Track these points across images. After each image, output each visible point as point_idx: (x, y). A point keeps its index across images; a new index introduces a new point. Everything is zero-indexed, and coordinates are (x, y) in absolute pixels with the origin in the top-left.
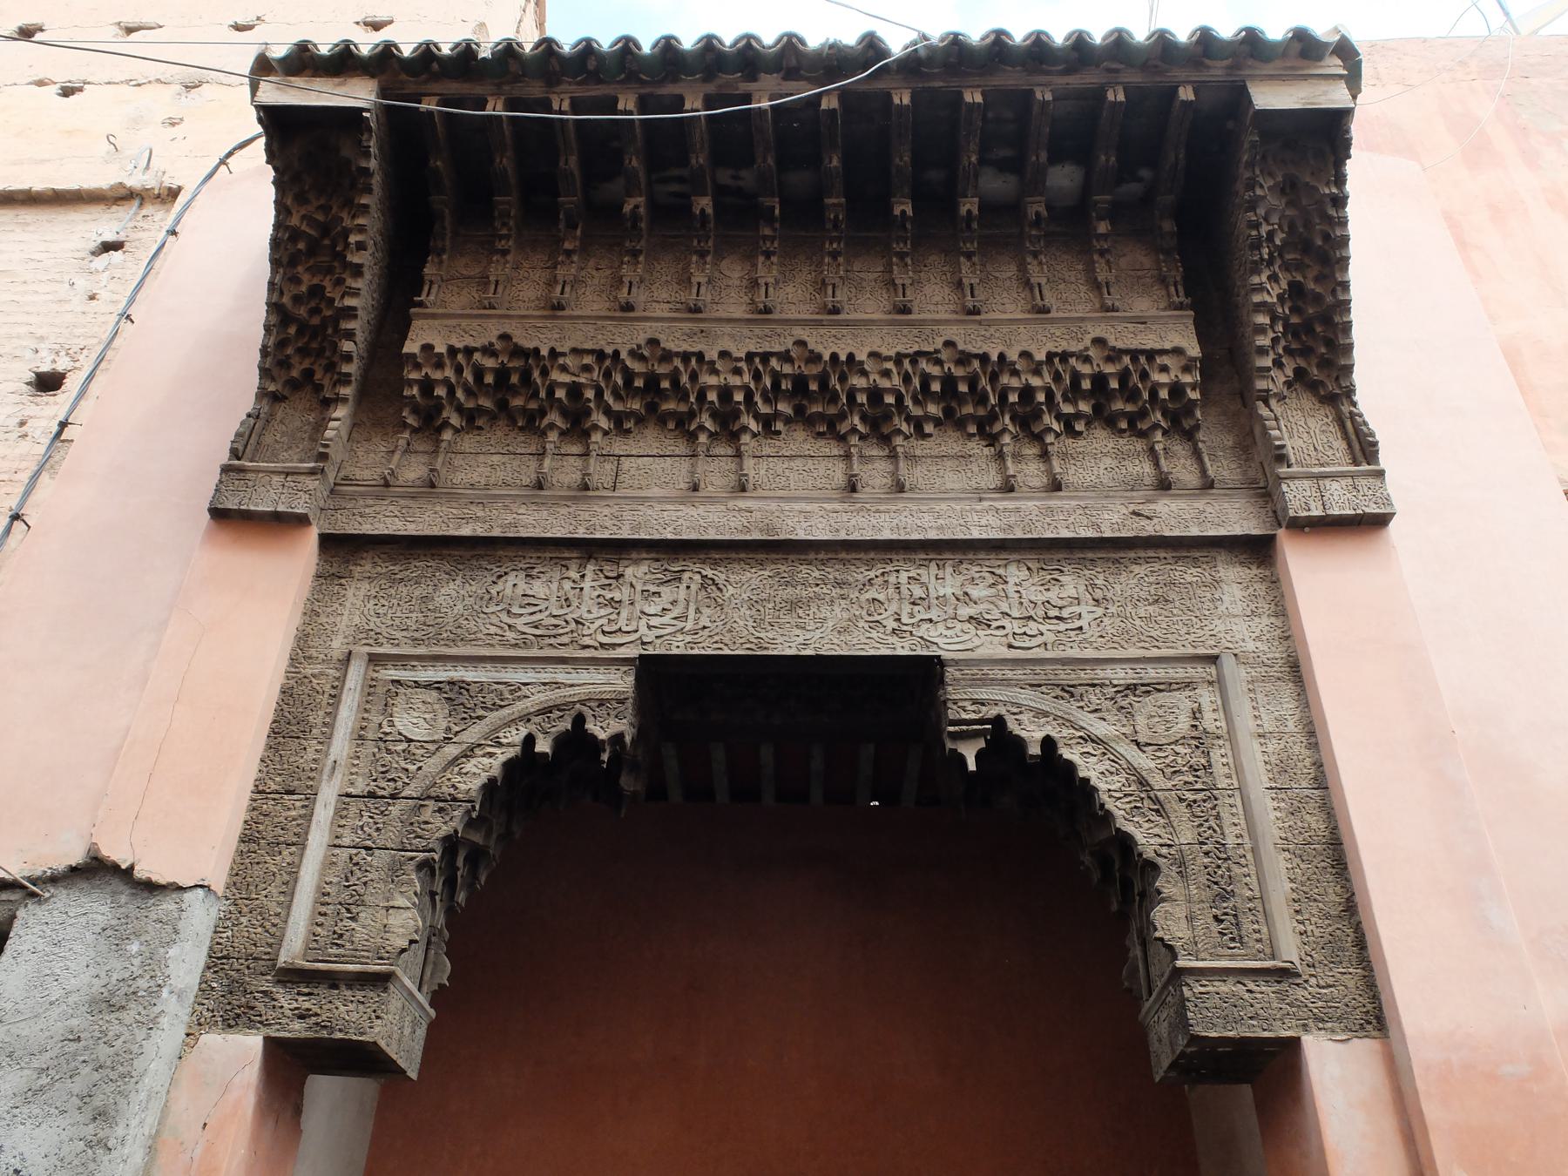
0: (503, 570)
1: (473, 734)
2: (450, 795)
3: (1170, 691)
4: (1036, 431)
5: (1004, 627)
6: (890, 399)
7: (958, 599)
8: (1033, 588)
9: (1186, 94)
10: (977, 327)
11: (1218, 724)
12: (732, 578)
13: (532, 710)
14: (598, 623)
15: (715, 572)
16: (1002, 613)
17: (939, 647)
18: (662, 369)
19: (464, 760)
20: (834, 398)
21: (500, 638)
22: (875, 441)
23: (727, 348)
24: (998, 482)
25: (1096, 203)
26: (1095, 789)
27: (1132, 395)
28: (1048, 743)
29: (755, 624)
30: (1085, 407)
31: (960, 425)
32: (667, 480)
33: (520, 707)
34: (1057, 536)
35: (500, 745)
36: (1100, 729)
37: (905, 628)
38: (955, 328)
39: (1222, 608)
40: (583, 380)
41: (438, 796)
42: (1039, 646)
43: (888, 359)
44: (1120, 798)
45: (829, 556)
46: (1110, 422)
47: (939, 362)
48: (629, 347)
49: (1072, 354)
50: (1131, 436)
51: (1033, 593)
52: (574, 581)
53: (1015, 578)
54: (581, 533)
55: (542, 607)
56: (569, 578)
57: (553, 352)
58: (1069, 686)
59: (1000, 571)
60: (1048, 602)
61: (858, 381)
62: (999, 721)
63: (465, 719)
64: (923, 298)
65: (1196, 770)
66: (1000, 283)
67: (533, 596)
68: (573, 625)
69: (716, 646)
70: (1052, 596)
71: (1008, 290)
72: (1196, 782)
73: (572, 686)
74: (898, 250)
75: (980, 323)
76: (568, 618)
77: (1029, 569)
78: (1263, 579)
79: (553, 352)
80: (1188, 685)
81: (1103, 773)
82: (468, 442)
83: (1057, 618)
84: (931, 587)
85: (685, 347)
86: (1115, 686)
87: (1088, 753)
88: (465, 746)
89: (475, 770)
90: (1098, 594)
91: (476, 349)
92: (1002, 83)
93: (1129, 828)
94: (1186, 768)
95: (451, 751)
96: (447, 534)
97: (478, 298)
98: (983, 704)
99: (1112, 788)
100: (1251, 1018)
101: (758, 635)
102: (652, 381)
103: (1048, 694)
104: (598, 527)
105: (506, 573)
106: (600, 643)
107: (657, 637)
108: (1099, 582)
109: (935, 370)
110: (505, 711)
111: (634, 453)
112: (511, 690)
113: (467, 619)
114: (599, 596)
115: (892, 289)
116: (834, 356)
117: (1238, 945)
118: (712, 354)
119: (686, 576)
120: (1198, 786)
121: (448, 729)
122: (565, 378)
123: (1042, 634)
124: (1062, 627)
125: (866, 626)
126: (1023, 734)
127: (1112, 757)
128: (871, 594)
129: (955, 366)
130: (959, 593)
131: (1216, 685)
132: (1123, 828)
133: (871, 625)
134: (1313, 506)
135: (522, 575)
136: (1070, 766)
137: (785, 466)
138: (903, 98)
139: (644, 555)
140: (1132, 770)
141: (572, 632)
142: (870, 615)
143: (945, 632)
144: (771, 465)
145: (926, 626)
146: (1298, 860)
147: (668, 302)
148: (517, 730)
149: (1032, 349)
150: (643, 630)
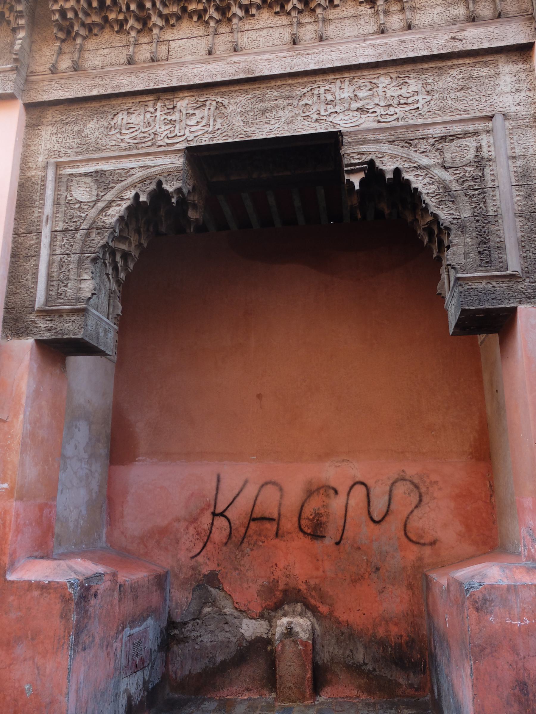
0: (116, 111)
1: (109, 196)
5: (376, 112)
7: (351, 99)
8: (393, 88)
11: (490, 153)
12: (232, 101)
13: (136, 181)
14: (165, 133)
19: (107, 209)
22: (307, 13)
26: (421, 193)
28: (397, 172)
29: (244, 124)
35: (122, 199)
36: (425, 161)
37: (322, 118)
51: (393, 91)
52: (152, 113)
54: (152, 86)
58: (412, 140)
59: (374, 81)
60: (401, 95)
62: (371, 163)
65: (476, 179)
68: (152, 136)
69: (224, 138)
70: (403, 92)
72: (475, 185)
76: (150, 132)
77: (391, 78)
82: (90, 44)
84: (337, 94)
86: (435, 138)
87: (418, 175)
88: (107, 202)
90: (429, 88)
94: (470, 178)
95: (101, 205)
98: (363, 154)
99: (430, 191)
100: (493, 299)
101: (245, 130)
103: (398, 145)
104: (160, 82)
105: (118, 113)
106: (167, 144)
111: (176, 38)
114: (165, 119)
120: (476, 187)
124: (408, 108)
126: (384, 168)
127: (431, 176)
130: (352, 95)
133: (305, 118)
135: (125, 113)
136: (408, 182)
141: (153, 139)
144: (250, 35)
145: (333, 115)
150: (187, 134)
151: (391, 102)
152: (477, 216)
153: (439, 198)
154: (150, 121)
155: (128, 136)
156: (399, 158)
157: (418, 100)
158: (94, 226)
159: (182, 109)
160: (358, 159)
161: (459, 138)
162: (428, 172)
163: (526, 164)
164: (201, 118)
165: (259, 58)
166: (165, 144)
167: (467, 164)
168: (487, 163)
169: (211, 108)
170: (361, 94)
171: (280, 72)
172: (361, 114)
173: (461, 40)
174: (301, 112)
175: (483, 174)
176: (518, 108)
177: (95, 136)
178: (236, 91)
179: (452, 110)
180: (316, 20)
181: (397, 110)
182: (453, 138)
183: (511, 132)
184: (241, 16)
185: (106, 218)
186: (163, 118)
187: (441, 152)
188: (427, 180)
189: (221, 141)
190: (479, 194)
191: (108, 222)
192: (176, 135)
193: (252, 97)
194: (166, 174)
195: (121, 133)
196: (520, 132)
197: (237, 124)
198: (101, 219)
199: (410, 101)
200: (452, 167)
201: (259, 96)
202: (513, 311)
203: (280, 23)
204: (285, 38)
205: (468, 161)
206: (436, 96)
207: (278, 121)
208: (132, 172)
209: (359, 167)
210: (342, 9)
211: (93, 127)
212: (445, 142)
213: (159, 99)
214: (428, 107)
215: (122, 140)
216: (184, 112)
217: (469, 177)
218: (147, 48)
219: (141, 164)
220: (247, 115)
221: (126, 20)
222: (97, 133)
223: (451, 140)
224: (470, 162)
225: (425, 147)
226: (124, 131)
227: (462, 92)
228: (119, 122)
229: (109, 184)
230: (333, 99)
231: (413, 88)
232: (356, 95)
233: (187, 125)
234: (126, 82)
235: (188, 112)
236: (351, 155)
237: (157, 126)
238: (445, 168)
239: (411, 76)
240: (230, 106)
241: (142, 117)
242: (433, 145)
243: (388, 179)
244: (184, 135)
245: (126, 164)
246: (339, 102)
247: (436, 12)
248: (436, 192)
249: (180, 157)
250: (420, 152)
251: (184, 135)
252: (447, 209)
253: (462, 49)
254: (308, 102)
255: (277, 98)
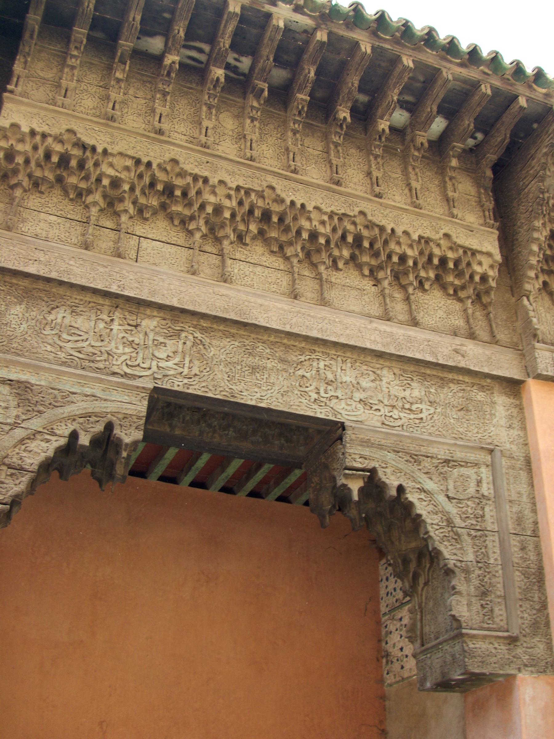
0: (56, 304)
1: (36, 424)
2: (19, 465)
3: (467, 467)
4: (403, 284)
5: (379, 410)
6: (322, 241)
7: (353, 386)
8: (397, 387)
9: (522, 102)
10: (379, 206)
11: (489, 491)
12: (214, 342)
13: (77, 413)
14: (123, 358)
15: (203, 336)
16: (379, 400)
17: (342, 416)
18: (179, 182)
19: (28, 441)
20: (287, 230)
21: (54, 355)
22: (307, 265)
23: (224, 179)
24: (380, 312)
25: (455, 147)
26: (424, 521)
27: (460, 274)
28: (401, 489)
29: (229, 379)
30: (432, 275)
31: (359, 267)
32: (173, 262)
33: (69, 410)
34: (413, 357)
35: (53, 434)
36: (430, 485)
37: (322, 399)
38: (366, 203)
39: (495, 421)
40: (123, 177)
41: (10, 464)
42: (399, 426)
43: (325, 213)
44: (437, 530)
45: (277, 340)
46: (444, 287)
47: (354, 223)
48: (159, 161)
49: (432, 240)
50: (453, 299)
51: (396, 390)
52: (106, 323)
53: (387, 378)
54: (114, 289)
55: (84, 338)
56: (103, 320)
57: (105, 152)
58: (416, 455)
59: (379, 372)
60: (404, 398)
61: (306, 224)
62: (373, 471)
63: (29, 411)
64: (347, 177)
65: (477, 518)
66: (392, 180)
67: (78, 328)
68: (105, 356)
69: (203, 389)
70: (407, 393)
71: (396, 185)
72: (477, 525)
73: (105, 400)
74: (335, 140)
75: (381, 204)
76: (103, 349)
77: (394, 374)
78: (516, 406)
79: (105, 152)
80: (476, 464)
81: (429, 513)
82: (34, 201)
83: (410, 410)
84: (338, 374)
85: (196, 171)
86: (439, 459)
87: (422, 499)
88: (29, 431)
89: (36, 450)
90: (432, 398)
91: (50, 136)
92: (425, 59)
93: (442, 548)
94: (472, 516)
95: (19, 433)
96: (19, 269)
97: (51, 97)
98: (366, 459)
99: (434, 522)
100: (495, 663)
101: (231, 387)
102: (169, 190)
103: (403, 458)
104: (126, 287)
105: (57, 307)
106: (125, 373)
107: (164, 376)
108: (433, 390)
109: (350, 227)
110: (60, 410)
111: (149, 236)
112: (63, 396)
113: (30, 336)
114: (123, 337)
115: (328, 166)
116: (293, 203)
117: (491, 622)
118: (214, 180)
119: (183, 335)
120: (478, 528)
121: (17, 417)
122: (111, 172)
123: (401, 419)
124: (412, 416)
125: (299, 393)
126: (387, 481)
127: (435, 504)
128: (301, 372)
129: (364, 228)
130: (354, 382)
131: (490, 467)
132: (438, 548)
133: (302, 393)
134: (549, 369)
135: (69, 311)
136: (410, 505)
137: (250, 270)
138: (366, 47)
139: (155, 313)
140: (445, 513)
141: (105, 360)
142: (301, 386)
143: (346, 407)
144: (242, 267)
145: (334, 401)
146: (523, 577)
147: (185, 135)
148: (66, 425)
149: (410, 230)
150: (154, 368)
151: (395, 404)
152: (480, 563)
153: (442, 533)
154: (103, 333)
155: (70, 345)
156: (403, 474)
157: (422, 410)
158: (6, 461)
159: (148, 330)
160: (361, 463)
161: (462, 466)
162: (431, 498)
163: (520, 512)
164: (174, 353)
165: (252, 300)
166: (123, 373)
167: (469, 498)
168: (488, 502)
169: (188, 342)
170: (365, 383)
171: (277, 328)
172: (364, 409)
173: (463, 356)
174: (297, 384)
175: (483, 513)
176: (512, 446)
177: (22, 329)
178: (220, 330)
179: (455, 432)
180: (317, 277)
181: (402, 415)
182: (456, 464)
183: (507, 471)
184: (204, 232)
185: (25, 454)
186: (121, 335)
187: (445, 477)
188: (430, 508)
189: (199, 393)
190: (481, 537)
191: (29, 461)
192: (138, 365)
193: (239, 345)
194: (120, 416)
195: (60, 336)
196: (515, 474)
197: (220, 376)
198: (18, 453)
199: (414, 407)
200: (455, 499)
201: (248, 347)
202: (510, 678)
203: (276, 265)
204: (283, 286)
205: (470, 496)
206: (439, 410)
207: (269, 387)
208: (72, 398)
209: (361, 473)
210: (345, 275)
211: (21, 315)
212: (448, 467)
213: (117, 307)
214: (432, 421)
215: (61, 347)
216: (151, 336)
217: (471, 514)
218: (109, 236)
219: (88, 391)
220: (232, 368)
221: (89, 192)
222: (24, 325)
223: (453, 466)
224: (472, 497)
225: (429, 467)
226: (65, 336)
227: (462, 413)
228: (59, 320)
229: (36, 406)
230: (333, 380)
231: (416, 393)
232: (358, 383)
233: (153, 355)
234: (77, 271)
235: (155, 338)
236: (353, 456)
237: (113, 344)
238: (448, 497)
239: (415, 379)
240: (212, 349)
241: (92, 324)
242: (437, 467)
243: (391, 496)
244: (150, 368)
245: (68, 385)
246: (340, 385)
247: (439, 316)
248: (440, 524)
249: (142, 397)
250: (424, 471)
251: (150, 368)
252: (450, 548)
253: (465, 366)
254: (306, 374)
255: (270, 357)
